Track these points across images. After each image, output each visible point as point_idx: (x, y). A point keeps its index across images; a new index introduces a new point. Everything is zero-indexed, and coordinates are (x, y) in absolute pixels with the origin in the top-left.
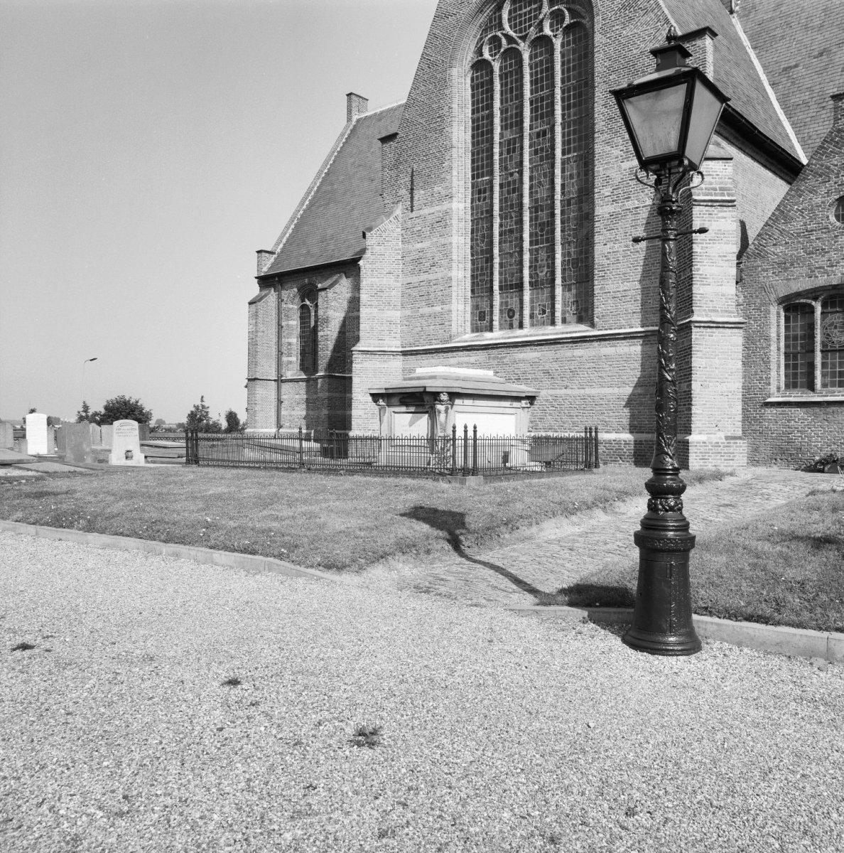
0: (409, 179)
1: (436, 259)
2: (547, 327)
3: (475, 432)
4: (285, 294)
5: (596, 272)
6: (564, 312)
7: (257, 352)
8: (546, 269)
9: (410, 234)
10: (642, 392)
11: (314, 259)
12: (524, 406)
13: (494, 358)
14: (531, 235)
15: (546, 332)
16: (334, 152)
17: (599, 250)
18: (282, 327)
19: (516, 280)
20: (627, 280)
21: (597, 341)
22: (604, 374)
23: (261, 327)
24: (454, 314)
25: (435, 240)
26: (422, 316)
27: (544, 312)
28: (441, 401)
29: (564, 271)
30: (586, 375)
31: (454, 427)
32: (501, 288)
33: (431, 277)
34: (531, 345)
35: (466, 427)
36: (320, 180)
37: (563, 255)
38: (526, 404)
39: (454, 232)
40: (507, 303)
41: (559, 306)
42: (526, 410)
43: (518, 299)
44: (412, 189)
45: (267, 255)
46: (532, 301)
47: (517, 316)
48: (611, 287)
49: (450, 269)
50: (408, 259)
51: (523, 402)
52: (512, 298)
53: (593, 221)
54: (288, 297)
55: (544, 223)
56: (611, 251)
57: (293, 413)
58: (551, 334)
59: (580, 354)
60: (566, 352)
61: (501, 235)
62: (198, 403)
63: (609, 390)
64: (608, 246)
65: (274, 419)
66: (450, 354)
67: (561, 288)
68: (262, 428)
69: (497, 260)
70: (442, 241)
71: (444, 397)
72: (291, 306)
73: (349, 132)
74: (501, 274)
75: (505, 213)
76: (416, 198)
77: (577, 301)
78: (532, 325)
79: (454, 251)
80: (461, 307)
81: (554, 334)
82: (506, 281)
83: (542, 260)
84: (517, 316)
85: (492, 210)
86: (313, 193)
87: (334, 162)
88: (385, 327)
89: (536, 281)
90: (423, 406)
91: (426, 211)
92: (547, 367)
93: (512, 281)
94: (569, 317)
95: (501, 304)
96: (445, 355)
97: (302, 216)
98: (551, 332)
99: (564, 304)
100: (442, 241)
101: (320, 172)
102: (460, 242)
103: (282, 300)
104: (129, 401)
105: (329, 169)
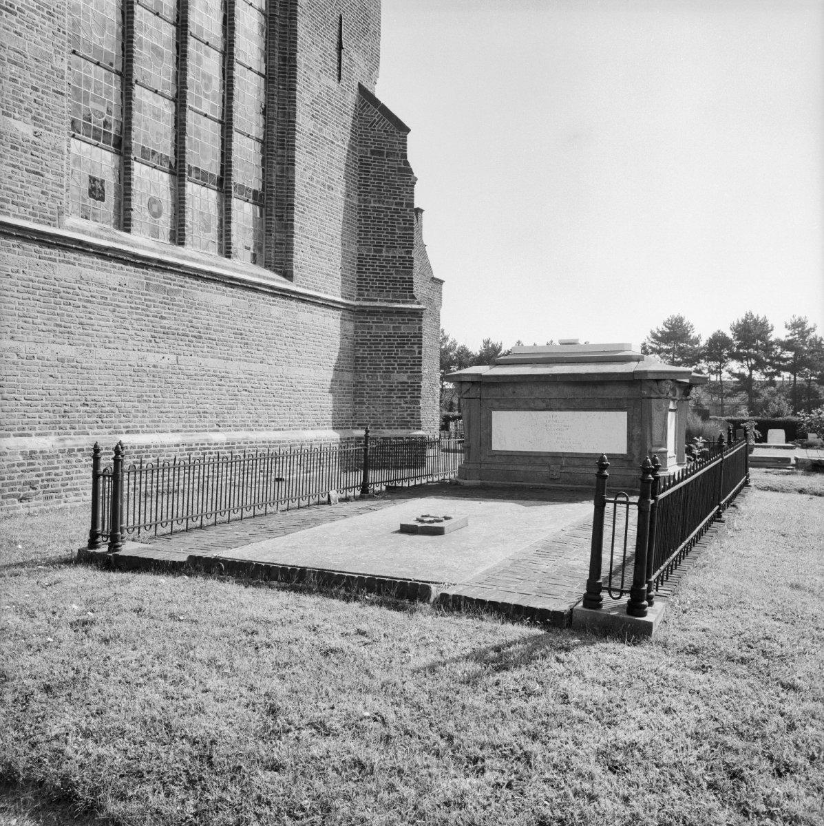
13: (157, 289)
34: (219, 282)
66: (55, 253)
92: (239, 324)
96: (46, 251)
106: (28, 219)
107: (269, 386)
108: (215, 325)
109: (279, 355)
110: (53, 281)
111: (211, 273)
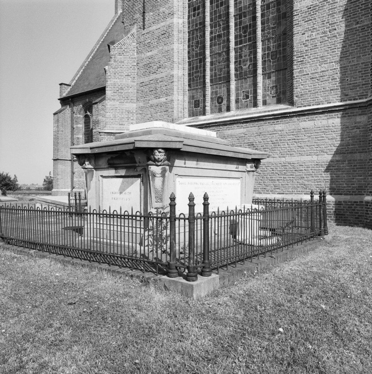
0: (141, 6)
1: (161, 62)
2: (250, 109)
3: (206, 205)
4: (75, 109)
5: (295, 58)
6: (264, 96)
7: (58, 143)
8: (248, 63)
9: (143, 46)
10: (341, 158)
11: (92, 87)
12: (249, 169)
14: (236, 37)
15: (250, 112)
16: (107, 30)
17: (298, 39)
18: (74, 128)
19: (224, 73)
20: (325, 62)
21: (296, 116)
22: (303, 145)
23: (61, 128)
24: (175, 103)
25: (161, 48)
26: (152, 106)
27: (247, 97)
28: (155, 160)
29: (264, 62)
30: (287, 146)
31: (173, 199)
32: (211, 81)
33: (158, 76)
35: (191, 199)
36: (99, 45)
37: (263, 50)
38: (251, 167)
39: (175, 40)
40: (216, 92)
41: (260, 91)
42: (251, 173)
43: (225, 89)
44: (144, 12)
45: (66, 86)
46: (237, 89)
47: (225, 102)
48: (309, 69)
49: (172, 69)
50: (141, 65)
51: (249, 165)
52: (220, 88)
53: (292, 16)
54: (77, 110)
55: (247, 26)
56: (309, 39)
57: (80, 179)
58: (255, 113)
59: (280, 128)
60: (267, 127)
61: (211, 40)
62: (48, 175)
63: (309, 158)
64: (306, 35)
65: (69, 183)
67: (262, 77)
68: (62, 188)
69: (208, 60)
70: (166, 48)
71: (160, 155)
72: (79, 116)
73: (116, 19)
74: (211, 70)
75: (215, 23)
76: (147, 19)
77: (276, 86)
78: (238, 108)
79: (175, 55)
80: (181, 98)
81: (258, 113)
82: (215, 75)
83: (245, 56)
84: (225, 102)
85: (204, 22)
86: (94, 52)
87: (107, 35)
88: (125, 116)
89: (241, 73)
90: (135, 167)
91: (154, 27)
92: (251, 140)
93: (221, 75)
94: (268, 100)
95: (212, 93)
97: (88, 65)
98: (255, 111)
99: (265, 90)
100: (166, 48)
101: (99, 41)
102: (180, 48)
103: (74, 113)
104: (3, 174)
105: (104, 39)
106: (301, 107)
107: (274, 170)
108: (237, 144)
109: (281, 151)
110: (331, 127)
111: (231, 121)
